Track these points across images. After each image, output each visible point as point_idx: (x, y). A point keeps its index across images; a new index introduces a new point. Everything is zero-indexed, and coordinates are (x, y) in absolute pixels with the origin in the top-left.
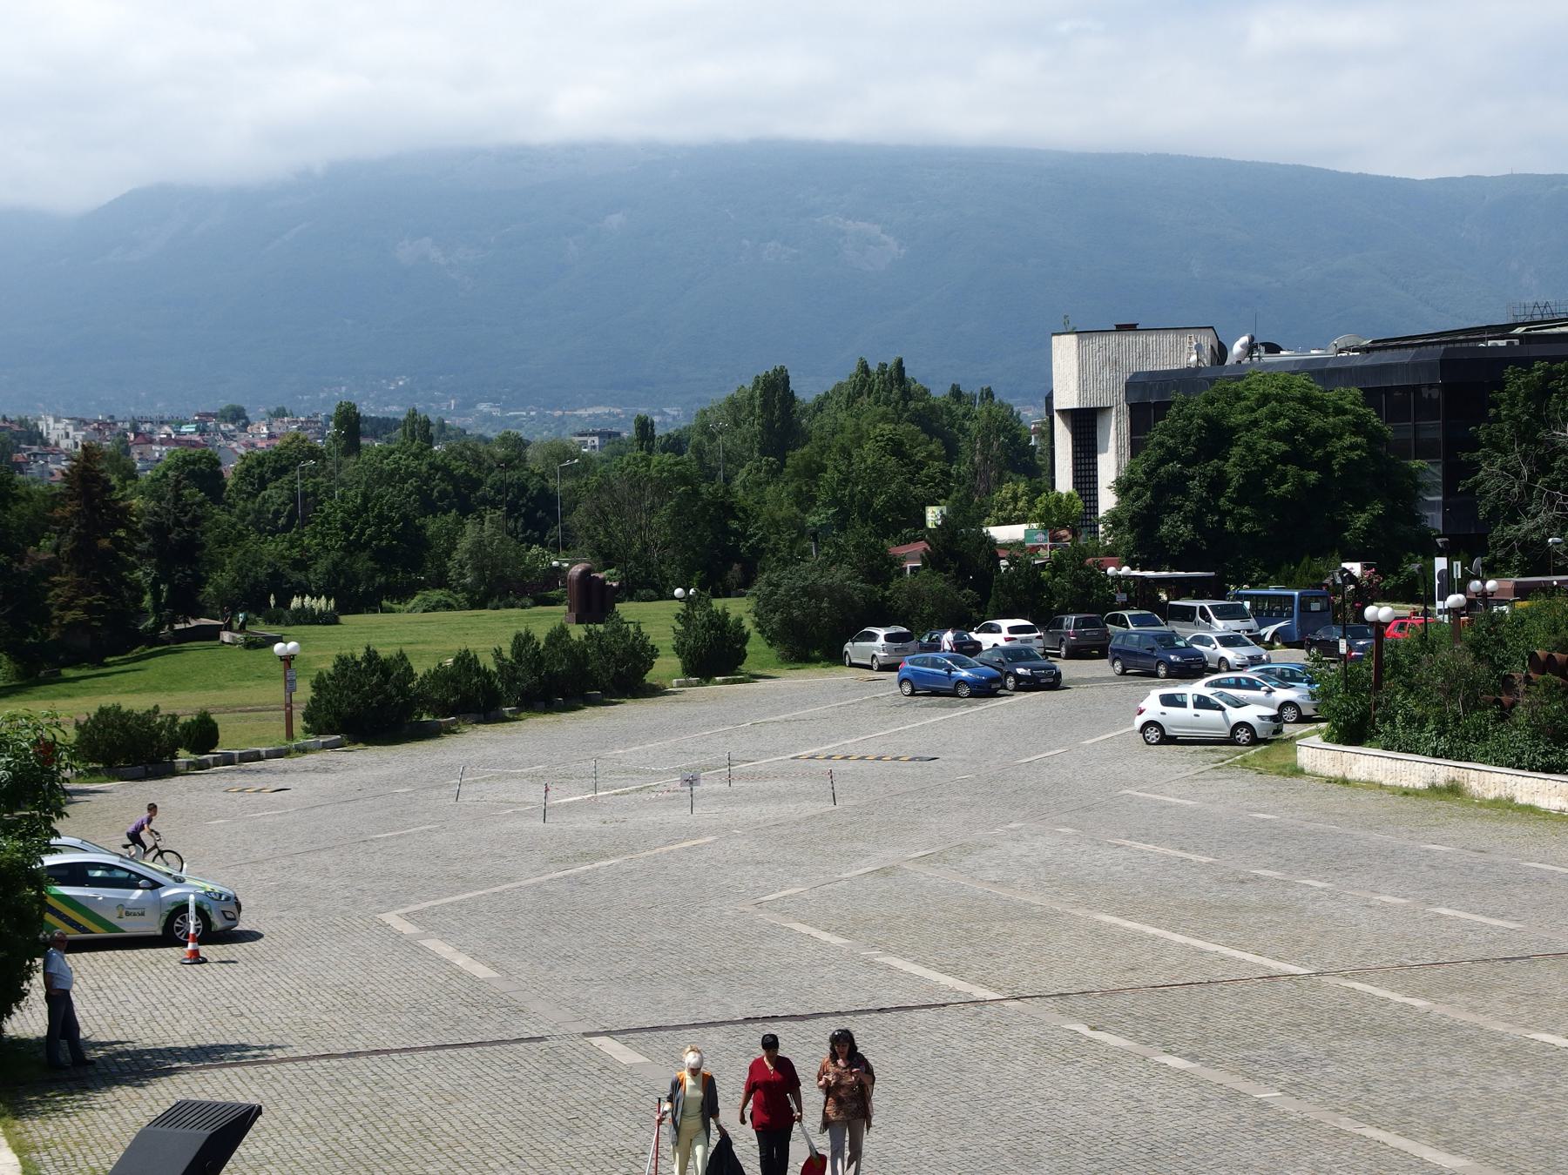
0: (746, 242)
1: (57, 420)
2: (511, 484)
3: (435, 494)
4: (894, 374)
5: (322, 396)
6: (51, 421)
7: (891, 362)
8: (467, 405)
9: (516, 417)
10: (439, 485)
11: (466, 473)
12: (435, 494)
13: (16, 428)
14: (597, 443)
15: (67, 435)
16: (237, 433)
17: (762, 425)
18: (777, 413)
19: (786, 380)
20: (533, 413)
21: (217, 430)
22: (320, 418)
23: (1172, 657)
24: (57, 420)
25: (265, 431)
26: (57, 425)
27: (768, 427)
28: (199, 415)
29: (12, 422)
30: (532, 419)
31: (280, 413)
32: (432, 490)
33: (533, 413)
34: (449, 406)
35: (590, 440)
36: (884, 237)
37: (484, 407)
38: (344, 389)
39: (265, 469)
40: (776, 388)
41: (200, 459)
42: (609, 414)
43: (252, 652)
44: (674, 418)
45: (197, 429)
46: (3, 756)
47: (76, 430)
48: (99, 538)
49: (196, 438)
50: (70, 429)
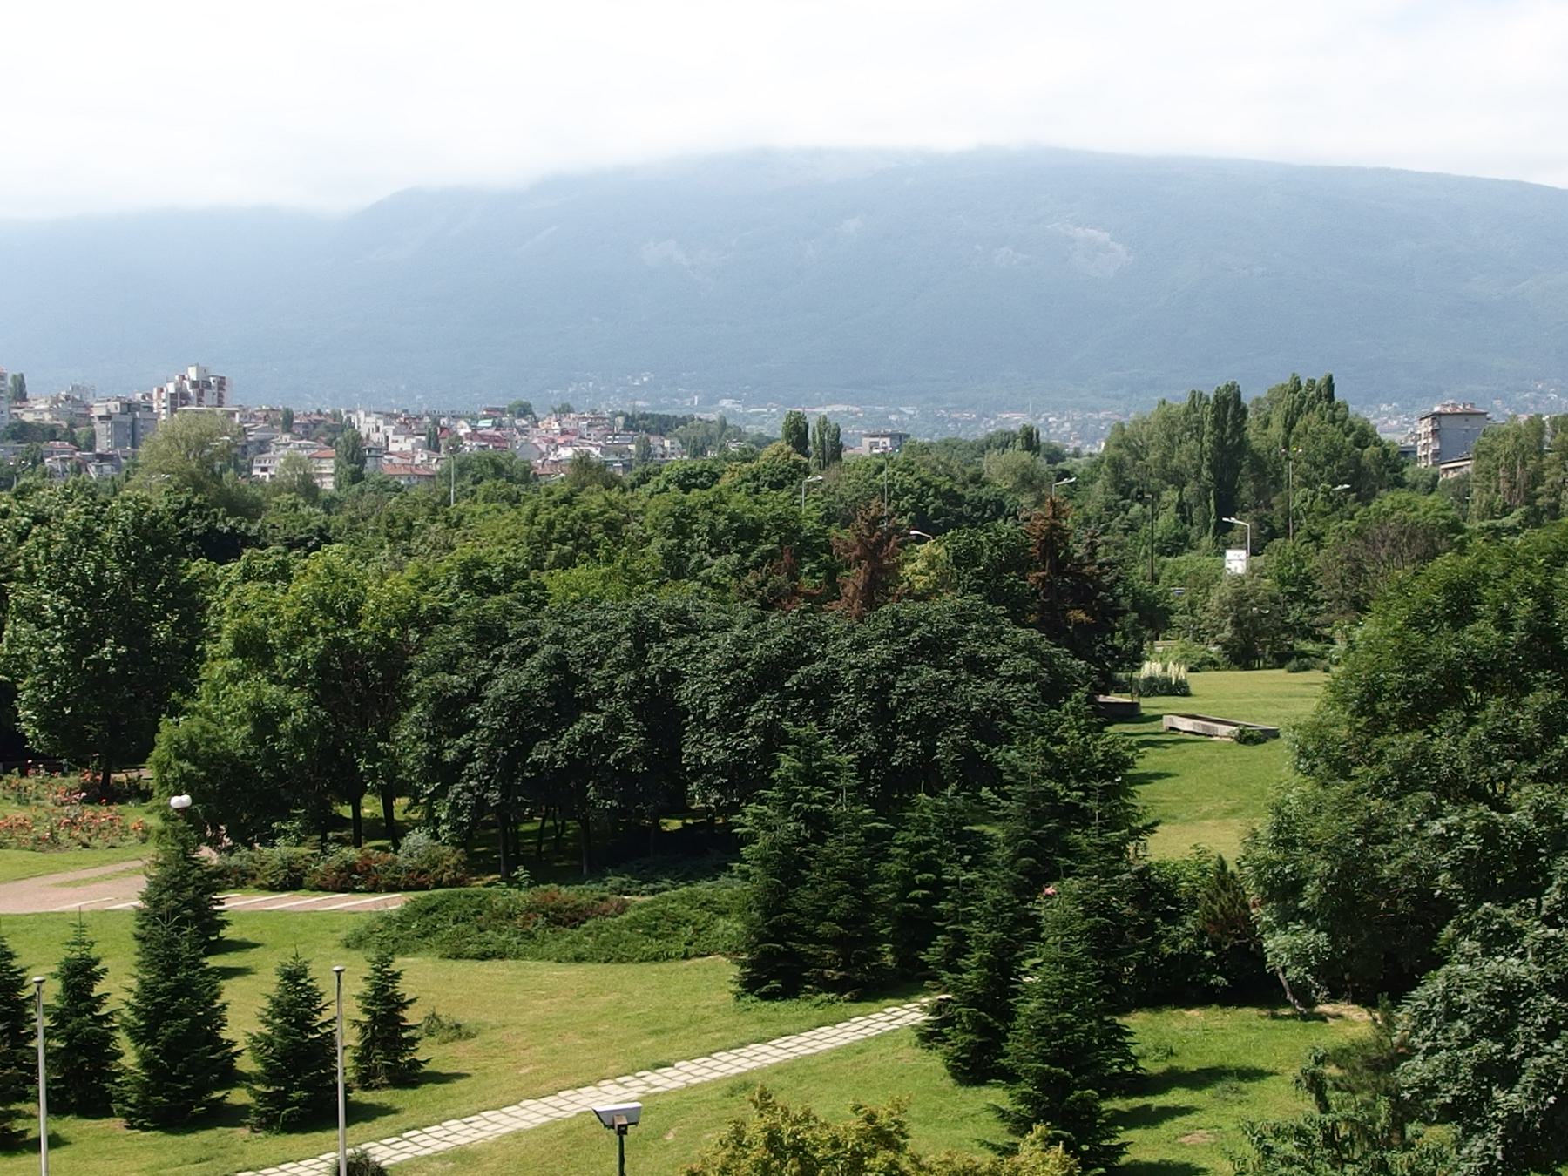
0: (978, 247)
1: (367, 415)
2: (988, 501)
3: (930, 512)
4: (1324, 391)
5: (570, 390)
6: (362, 415)
7: (1320, 379)
8: (711, 401)
9: (758, 414)
10: (933, 504)
11: (951, 489)
12: (930, 512)
13: (330, 421)
14: (888, 443)
15: (378, 429)
16: (529, 428)
17: (1214, 442)
18: (1228, 430)
19: (1238, 396)
20: (774, 410)
21: (512, 425)
22: (606, 415)
23: (1082, 616)
24: (367, 415)
25: (556, 426)
26: (368, 419)
27: (1219, 443)
28: (486, 410)
29: (327, 415)
30: (774, 415)
31: (566, 410)
32: (927, 507)
33: (774, 410)
34: (693, 402)
35: (881, 441)
36: (1112, 245)
37: (726, 403)
38: (591, 384)
39: (761, 483)
40: (1229, 406)
41: (701, 473)
42: (848, 412)
43: (1247, 750)
44: (911, 416)
45: (493, 423)
46: (1567, 1010)
47: (386, 424)
48: (1067, 610)
49: (491, 432)
50: (381, 423)
